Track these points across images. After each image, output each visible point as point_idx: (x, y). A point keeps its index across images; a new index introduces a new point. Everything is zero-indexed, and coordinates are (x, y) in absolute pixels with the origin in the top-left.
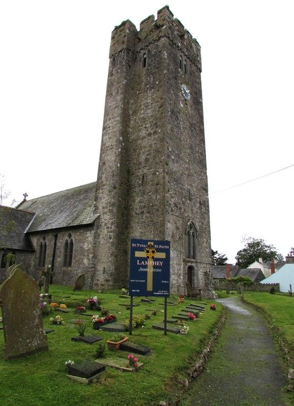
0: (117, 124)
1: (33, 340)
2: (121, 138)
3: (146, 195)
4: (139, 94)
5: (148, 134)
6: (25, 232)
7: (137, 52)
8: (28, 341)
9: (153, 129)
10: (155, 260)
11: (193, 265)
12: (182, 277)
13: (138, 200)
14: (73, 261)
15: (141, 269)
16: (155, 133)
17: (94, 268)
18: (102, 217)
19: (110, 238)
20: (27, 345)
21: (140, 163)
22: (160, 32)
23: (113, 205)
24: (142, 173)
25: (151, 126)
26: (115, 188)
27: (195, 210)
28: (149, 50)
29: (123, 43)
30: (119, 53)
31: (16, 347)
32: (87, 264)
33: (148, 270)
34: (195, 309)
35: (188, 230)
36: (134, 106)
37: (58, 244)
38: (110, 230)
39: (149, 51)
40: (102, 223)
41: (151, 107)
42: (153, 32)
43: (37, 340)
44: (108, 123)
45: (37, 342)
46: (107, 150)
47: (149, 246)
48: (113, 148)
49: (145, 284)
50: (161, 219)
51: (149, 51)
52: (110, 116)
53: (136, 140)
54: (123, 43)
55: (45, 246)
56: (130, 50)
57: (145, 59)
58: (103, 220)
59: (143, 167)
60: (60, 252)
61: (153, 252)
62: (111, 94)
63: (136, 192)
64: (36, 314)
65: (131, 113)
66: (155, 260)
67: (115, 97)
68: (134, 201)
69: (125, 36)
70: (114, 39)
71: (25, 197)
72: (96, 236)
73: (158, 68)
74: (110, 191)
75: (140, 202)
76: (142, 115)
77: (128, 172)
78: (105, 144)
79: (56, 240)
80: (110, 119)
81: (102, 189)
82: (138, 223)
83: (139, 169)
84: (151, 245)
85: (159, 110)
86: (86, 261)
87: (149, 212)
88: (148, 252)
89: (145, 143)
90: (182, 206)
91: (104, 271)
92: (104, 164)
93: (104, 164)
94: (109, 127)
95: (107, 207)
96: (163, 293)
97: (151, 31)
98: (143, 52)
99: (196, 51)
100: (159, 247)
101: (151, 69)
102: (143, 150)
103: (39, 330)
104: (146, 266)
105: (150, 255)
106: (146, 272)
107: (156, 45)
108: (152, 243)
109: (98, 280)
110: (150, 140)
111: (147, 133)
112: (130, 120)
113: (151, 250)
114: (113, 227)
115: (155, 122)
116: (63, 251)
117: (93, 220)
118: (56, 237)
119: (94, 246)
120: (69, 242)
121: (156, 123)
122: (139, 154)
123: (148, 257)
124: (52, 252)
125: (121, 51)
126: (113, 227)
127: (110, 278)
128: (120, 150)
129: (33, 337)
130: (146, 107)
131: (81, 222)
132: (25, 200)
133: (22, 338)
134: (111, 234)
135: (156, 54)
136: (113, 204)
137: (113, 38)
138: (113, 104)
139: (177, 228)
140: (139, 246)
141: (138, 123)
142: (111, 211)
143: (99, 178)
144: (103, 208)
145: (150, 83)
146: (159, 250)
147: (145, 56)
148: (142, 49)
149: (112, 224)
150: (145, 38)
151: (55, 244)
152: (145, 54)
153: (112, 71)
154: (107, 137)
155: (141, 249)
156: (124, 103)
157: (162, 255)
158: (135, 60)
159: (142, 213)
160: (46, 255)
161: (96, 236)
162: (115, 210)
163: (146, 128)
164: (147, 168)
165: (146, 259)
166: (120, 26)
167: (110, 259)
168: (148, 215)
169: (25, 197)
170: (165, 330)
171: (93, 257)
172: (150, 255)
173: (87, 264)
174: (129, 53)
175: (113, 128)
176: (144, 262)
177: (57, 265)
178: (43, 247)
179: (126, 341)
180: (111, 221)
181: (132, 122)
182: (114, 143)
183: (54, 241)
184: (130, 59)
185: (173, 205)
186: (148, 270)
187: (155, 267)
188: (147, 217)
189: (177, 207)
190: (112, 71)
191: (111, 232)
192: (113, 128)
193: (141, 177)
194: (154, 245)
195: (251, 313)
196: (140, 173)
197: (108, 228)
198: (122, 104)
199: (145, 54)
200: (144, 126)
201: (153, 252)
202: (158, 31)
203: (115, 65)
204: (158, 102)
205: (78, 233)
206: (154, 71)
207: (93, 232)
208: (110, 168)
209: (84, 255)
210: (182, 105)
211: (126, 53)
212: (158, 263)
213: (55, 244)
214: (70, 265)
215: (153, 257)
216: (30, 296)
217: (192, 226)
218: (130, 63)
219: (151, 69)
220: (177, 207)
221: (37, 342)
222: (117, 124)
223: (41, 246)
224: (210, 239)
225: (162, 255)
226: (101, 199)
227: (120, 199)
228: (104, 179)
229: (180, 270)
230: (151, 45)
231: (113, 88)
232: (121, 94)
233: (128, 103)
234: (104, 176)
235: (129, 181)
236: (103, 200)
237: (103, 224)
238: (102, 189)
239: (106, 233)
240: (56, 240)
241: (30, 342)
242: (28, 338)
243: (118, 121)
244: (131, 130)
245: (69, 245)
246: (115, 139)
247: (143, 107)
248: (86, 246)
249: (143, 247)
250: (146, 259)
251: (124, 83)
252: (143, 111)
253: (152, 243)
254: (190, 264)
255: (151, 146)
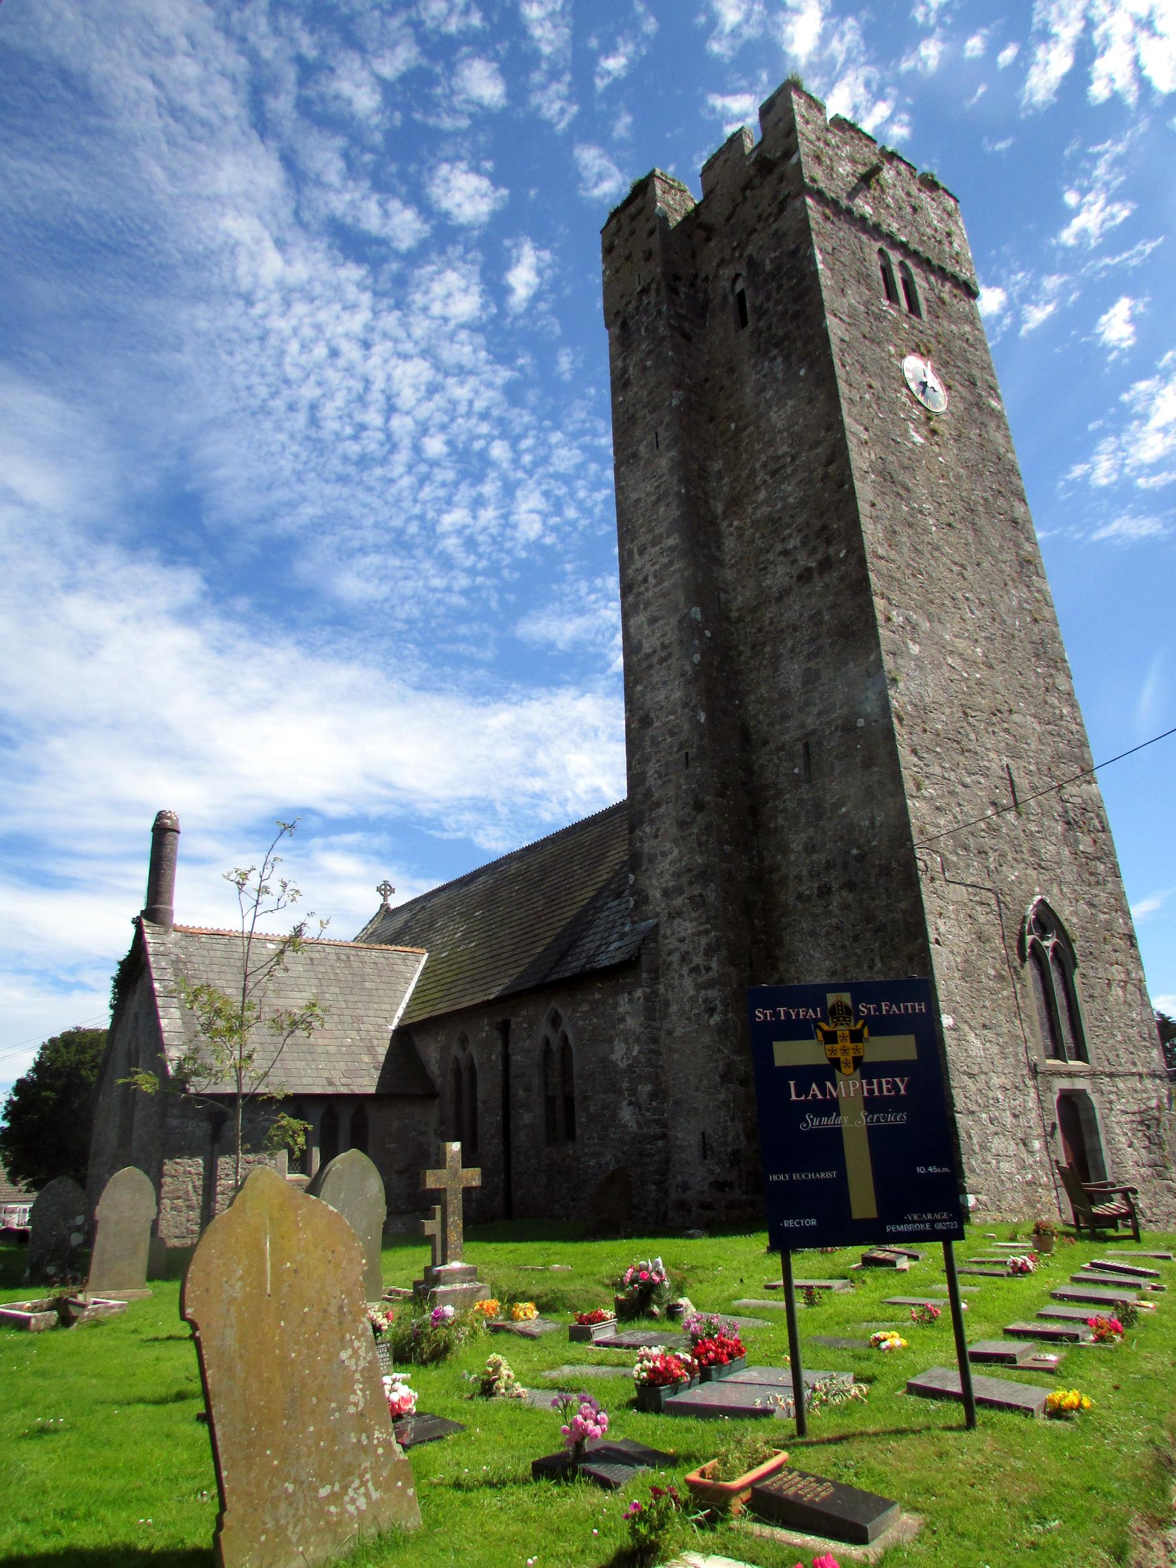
0: (671, 563)
1: (344, 1489)
2: (696, 613)
3: (830, 819)
4: (740, 430)
5: (800, 577)
6: (393, 1027)
7: (706, 279)
8: (324, 1492)
9: (814, 551)
10: (870, 1071)
11: (1081, 1084)
12: (1037, 1145)
13: (797, 842)
14: (581, 1118)
15: (813, 1122)
16: (826, 564)
17: (664, 1136)
18: (665, 930)
19: (711, 1011)
20: (321, 1513)
21: (785, 695)
22: (781, 180)
23: (703, 875)
24: (798, 734)
25: (804, 544)
26: (699, 807)
27: (1048, 850)
28: (750, 257)
29: (648, 256)
30: (640, 300)
31: (270, 1525)
32: (633, 1126)
33: (844, 1120)
34: (1120, 1285)
35: (1029, 938)
36: (726, 480)
37: (517, 1058)
38: (705, 977)
39: (751, 263)
40: (669, 954)
41: (794, 471)
42: (752, 189)
43: (364, 1484)
44: (638, 565)
45: (367, 1495)
46: (650, 666)
47: (833, 1013)
48: (670, 655)
49: (840, 1188)
50: (902, 905)
51: (751, 263)
52: (644, 538)
53: (754, 610)
54: (648, 256)
55: (472, 1070)
56: (677, 278)
57: (741, 296)
58: (673, 943)
59: (800, 710)
60: (528, 1089)
61: (856, 1037)
62: (635, 455)
63: (784, 810)
64: (351, 1364)
65: (720, 508)
66: (870, 1071)
67: (649, 462)
68: (785, 850)
69: (651, 232)
70: (614, 254)
71: (385, 897)
72: (654, 1010)
73: (796, 315)
74: (682, 824)
75: (810, 849)
76: (765, 509)
77: (745, 735)
78: (640, 645)
79: (506, 1043)
80: (642, 551)
81: (652, 821)
82: (812, 934)
83: (785, 717)
84: (840, 1004)
85: (826, 477)
86: (627, 1115)
87: (850, 886)
88: (830, 1038)
89: (794, 610)
90: (988, 841)
91: (706, 1148)
92: (646, 722)
93: (646, 722)
94: (645, 580)
95: (679, 890)
96: (932, 1222)
97: (748, 186)
98: (727, 272)
99: (941, 220)
100: (879, 1009)
101: (769, 327)
102: (790, 644)
103: (369, 1437)
104: (831, 1106)
105: (845, 1049)
106: (836, 1135)
107: (776, 232)
108: (846, 998)
109: (685, 1187)
110: (809, 596)
111: (795, 572)
112: (718, 538)
113: (842, 1030)
114: (714, 965)
115: (818, 523)
116: (536, 1081)
117: (632, 947)
118: (505, 1029)
119: (651, 1051)
120: (555, 1044)
121: (824, 528)
122: (776, 658)
123: (835, 1063)
124: (498, 1094)
125: (645, 291)
126: (714, 965)
127: (733, 1176)
128: (697, 658)
129: (347, 1473)
130: (773, 474)
131: (591, 958)
132: (384, 908)
133: (295, 1482)
134: (712, 993)
135: (778, 268)
136: (704, 873)
137: (608, 250)
138: (644, 490)
139: (981, 937)
140: (787, 1014)
141: (752, 541)
142: (698, 902)
143: (635, 778)
144: (666, 893)
145: (775, 379)
146: (882, 1026)
147: (739, 286)
148: (722, 263)
149: (710, 951)
150: (728, 219)
151: (506, 1058)
152: (737, 276)
153: (625, 370)
154: (640, 618)
155: (800, 1031)
156: (685, 480)
157: (902, 1048)
158: (702, 309)
159: (825, 891)
160: (479, 1104)
161: (654, 1010)
162: (711, 896)
163: (785, 553)
164: (815, 710)
165: (826, 1072)
166: (628, 202)
167: (722, 1097)
168: (849, 897)
169: (385, 897)
170: (966, 1398)
171: (653, 1096)
172: (845, 1049)
173: (633, 1126)
174: (675, 291)
175: (660, 581)
176: (823, 1089)
177: (521, 1138)
178: (465, 1077)
179: (777, 1469)
180: (704, 941)
181: (730, 543)
182: (672, 637)
183: (499, 1047)
184: (683, 312)
185: (946, 843)
186: (844, 1120)
187: (872, 1104)
188: (846, 907)
189: (966, 848)
190: (625, 370)
191: (709, 985)
192: (660, 581)
193: (799, 746)
194: (855, 1002)
195: (1031, 333)
196: (791, 733)
197: (695, 970)
198: (680, 481)
199: (737, 276)
200: (779, 548)
201: (856, 1037)
202: (772, 179)
203: (630, 345)
204: (817, 444)
205: (585, 1007)
206: (781, 332)
207: (639, 993)
208: (672, 734)
209: (619, 1092)
210: (918, 439)
211: (663, 293)
212: (883, 1087)
213: (506, 1058)
214: (571, 1135)
215: (857, 1062)
216: (317, 1286)
217: (1046, 919)
218: (687, 326)
219: (769, 327)
220: (966, 848)
221: (367, 1495)
222: (671, 563)
223: (458, 1073)
224: (1140, 966)
225: (902, 1048)
226: (652, 859)
227: (727, 848)
228: (652, 780)
229: (1025, 1111)
230: (755, 236)
231: (638, 433)
232: (669, 448)
233: (703, 475)
234: (652, 769)
235: (749, 771)
236: (664, 865)
237: (675, 958)
238: (652, 821)
239: (692, 992)
240: (506, 1043)
241: (335, 1498)
242: (324, 1479)
243: (672, 549)
244: (729, 575)
245: (557, 1057)
246: (674, 621)
247: (761, 476)
248: (619, 1053)
249: (806, 1022)
250: (826, 1072)
251: (675, 402)
252: (762, 495)
253: (846, 998)
254: (1065, 1084)
255: (816, 619)
